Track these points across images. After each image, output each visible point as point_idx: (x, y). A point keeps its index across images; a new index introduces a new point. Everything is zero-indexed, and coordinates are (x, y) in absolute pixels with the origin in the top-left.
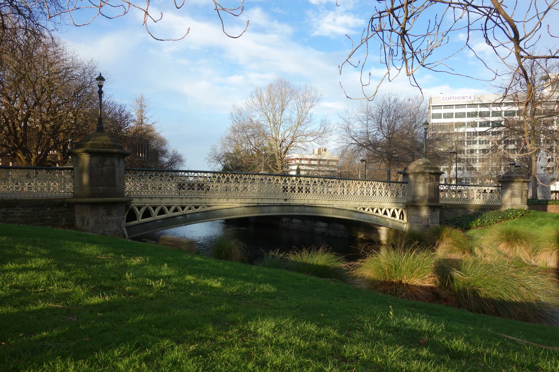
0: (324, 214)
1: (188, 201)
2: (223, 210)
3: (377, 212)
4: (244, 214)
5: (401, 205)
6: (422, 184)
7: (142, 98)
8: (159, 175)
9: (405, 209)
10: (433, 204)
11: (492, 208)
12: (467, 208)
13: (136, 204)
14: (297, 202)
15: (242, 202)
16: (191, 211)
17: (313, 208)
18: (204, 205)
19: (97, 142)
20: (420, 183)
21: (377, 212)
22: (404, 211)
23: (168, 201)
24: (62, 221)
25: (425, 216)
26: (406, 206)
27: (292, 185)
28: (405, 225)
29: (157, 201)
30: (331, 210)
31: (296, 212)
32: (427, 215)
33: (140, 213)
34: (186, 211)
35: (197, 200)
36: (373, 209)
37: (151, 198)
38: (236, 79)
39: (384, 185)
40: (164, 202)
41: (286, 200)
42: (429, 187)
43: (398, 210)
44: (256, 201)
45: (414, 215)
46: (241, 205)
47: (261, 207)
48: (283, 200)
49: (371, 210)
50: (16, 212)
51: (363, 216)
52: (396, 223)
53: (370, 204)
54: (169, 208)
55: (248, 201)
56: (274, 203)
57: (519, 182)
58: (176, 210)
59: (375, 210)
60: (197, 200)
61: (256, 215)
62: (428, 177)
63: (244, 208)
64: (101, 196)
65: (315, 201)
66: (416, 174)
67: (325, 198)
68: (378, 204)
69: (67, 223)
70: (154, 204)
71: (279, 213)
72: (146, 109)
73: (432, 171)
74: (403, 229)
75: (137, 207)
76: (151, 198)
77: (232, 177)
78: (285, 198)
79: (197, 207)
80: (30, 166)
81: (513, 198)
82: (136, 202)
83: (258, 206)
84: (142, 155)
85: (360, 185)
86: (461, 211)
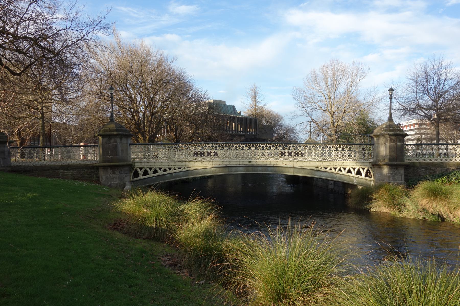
0: (286, 172)
1: (173, 164)
2: (199, 170)
3: (340, 170)
4: (216, 173)
5: (368, 164)
6: (383, 145)
7: (255, 87)
8: (174, 147)
9: (371, 168)
10: (392, 163)
12: (446, 166)
13: (138, 167)
16: (175, 171)
17: (275, 168)
18: (184, 166)
19: (107, 128)
20: (382, 144)
21: (340, 170)
22: (370, 170)
23: (159, 164)
24: (94, 177)
25: (387, 174)
26: (373, 166)
28: (372, 182)
29: (153, 164)
30: (292, 170)
32: (388, 173)
33: (141, 173)
34: (172, 171)
35: (180, 164)
36: (335, 169)
37: (148, 162)
39: (347, 147)
40: (156, 165)
41: (250, 162)
42: (390, 148)
43: (363, 169)
44: (225, 163)
45: (378, 173)
46: (212, 166)
47: (229, 168)
48: (248, 162)
49: (333, 170)
50: (68, 172)
51: (325, 174)
52: (361, 180)
53: (332, 164)
54: (160, 169)
55: (218, 163)
56: (240, 165)
58: (165, 170)
59: (337, 169)
60: (180, 164)
61: (260, 172)
62: (389, 139)
63: (215, 168)
64: (109, 161)
65: (277, 162)
66: (379, 136)
67: (346, 160)
68: (341, 164)
69: (97, 178)
70: (150, 167)
71: (245, 172)
72: (258, 95)
73: (391, 133)
74: (370, 186)
75: (139, 169)
76: (148, 162)
78: (249, 161)
79: (180, 168)
80: (145, 143)
82: (138, 166)
83: (226, 167)
84: (252, 130)
86: (440, 169)
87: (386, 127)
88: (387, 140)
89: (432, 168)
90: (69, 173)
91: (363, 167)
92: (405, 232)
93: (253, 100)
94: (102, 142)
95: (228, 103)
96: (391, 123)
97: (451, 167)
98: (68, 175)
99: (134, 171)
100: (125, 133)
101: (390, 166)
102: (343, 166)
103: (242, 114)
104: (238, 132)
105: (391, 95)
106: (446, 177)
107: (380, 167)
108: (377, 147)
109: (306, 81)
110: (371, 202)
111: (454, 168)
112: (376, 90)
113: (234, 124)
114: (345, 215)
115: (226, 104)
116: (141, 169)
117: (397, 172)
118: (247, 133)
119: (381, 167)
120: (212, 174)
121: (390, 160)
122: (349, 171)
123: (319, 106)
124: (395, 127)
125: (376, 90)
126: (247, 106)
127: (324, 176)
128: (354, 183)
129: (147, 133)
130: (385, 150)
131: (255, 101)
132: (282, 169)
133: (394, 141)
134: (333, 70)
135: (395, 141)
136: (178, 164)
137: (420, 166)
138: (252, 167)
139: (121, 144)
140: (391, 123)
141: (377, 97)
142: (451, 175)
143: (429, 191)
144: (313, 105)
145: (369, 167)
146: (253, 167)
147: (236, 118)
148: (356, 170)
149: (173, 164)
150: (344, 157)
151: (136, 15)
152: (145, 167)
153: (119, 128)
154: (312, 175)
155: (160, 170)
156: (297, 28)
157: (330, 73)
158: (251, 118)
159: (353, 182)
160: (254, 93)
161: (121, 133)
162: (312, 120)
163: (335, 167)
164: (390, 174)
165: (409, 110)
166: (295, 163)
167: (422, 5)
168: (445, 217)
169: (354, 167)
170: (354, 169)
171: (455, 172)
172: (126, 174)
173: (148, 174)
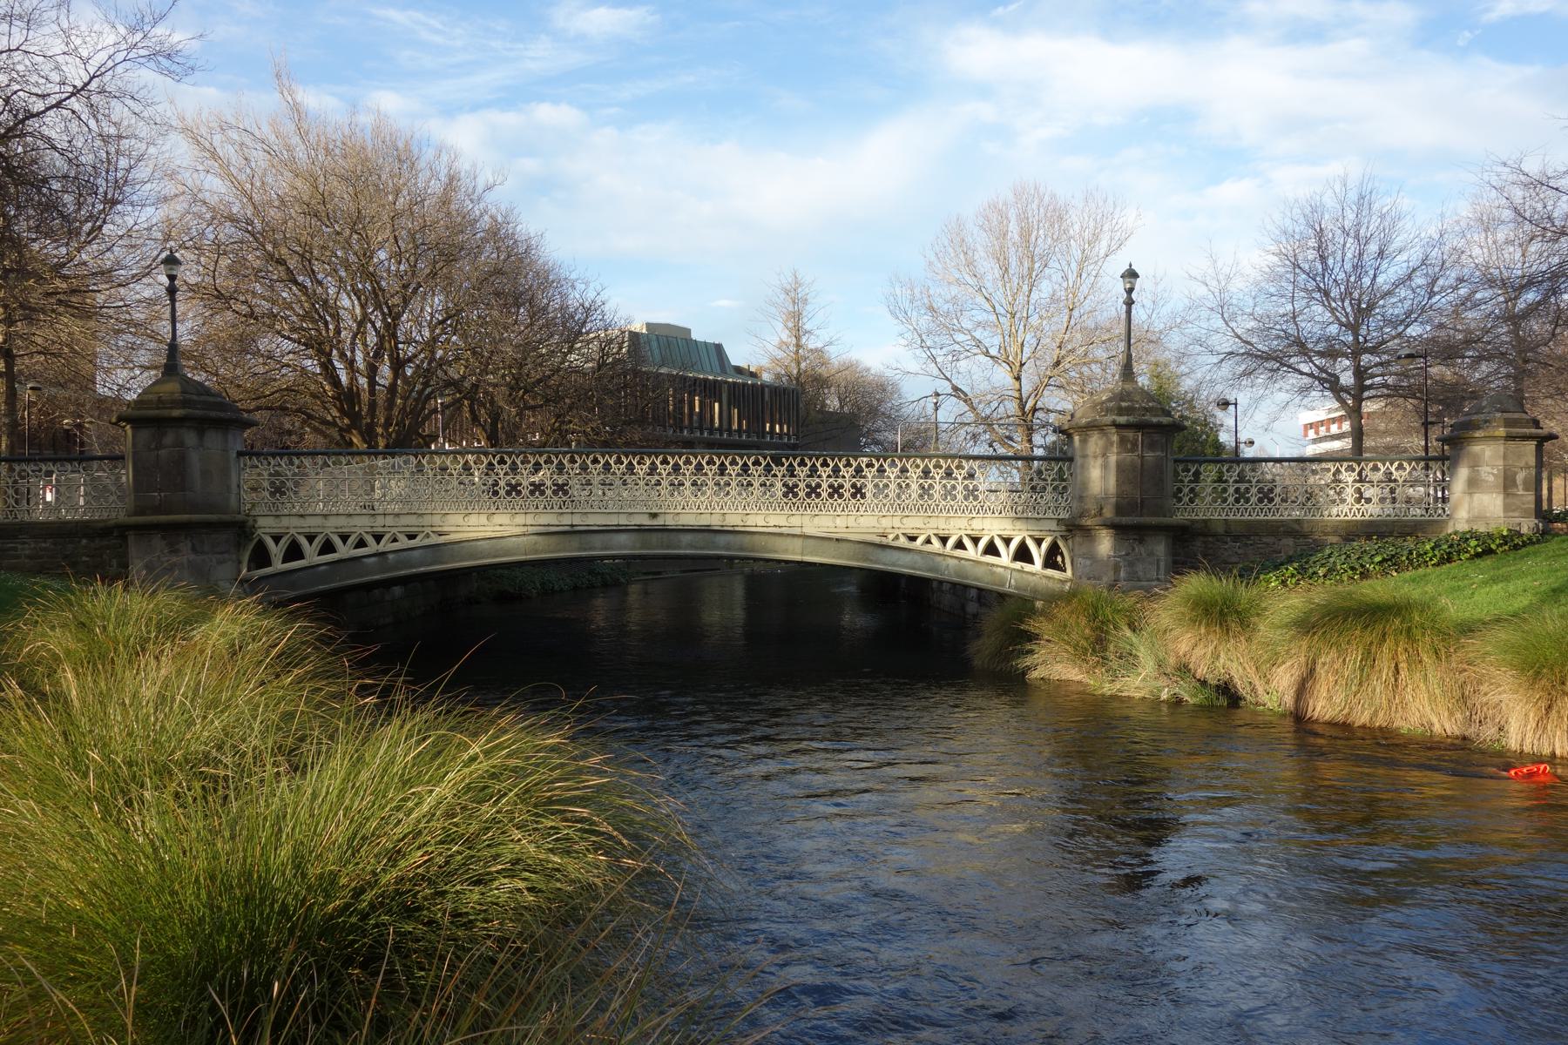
0: (776, 552)
1: (389, 521)
3: (960, 545)
4: (536, 552)
5: (1053, 526)
6: (1100, 461)
7: (797, 284)
10: (1125, 520)
11: (1408, 530)
13: (268, 530)
14: (688, 520)
15: (529, 522)
16: (396, 546)
18: (428, 530)
20: (1095, 457)
21: (960, 545)
22: (1061, 544)
23: (342, 521)
30: (798, 542)
31: (685, 546)
33: (276, 551)
34: (385, 545)
36: (944, 540)
37: (302, 516)
38: (1233, 191)
40: (331, 527)
41: (654, 516)
42: (1119, 465)
43: (1039, 542)
45: (1084, 556)
46: (525, 529)
47: (583, 536)
49: (936, 544)
50: (20, 546)
53: (933, 523)
55: (544, 519)
58: (361, 543)
59: (951, 543)
62: (1115, 438)
63: (535, 537)
64: (157, 510)
65: (745, 518)
68: (962, 523)
70: (307, 530)
72: (808, 308)
73: (1122, 420)
76: (302, 516)
77: (665, 462)
79: (412, 537)
81: (1476, 496)
82: (266, 525)
84: (781, 429)
86: (1290, 541)
87: (1110, 400)
88: (1112, 444)
89: (1265, 540)
90: (23, 549)
91: (1037, 534)
92: (291, 613)
93: (790, 325)
94: (134, 445)
96: (1126, 386)
97: (1326, 534)
98: (18, 557)
99: (251, 547)
100: (213, 414)
101: (1119, 530)
102: (970, 532)
103: (767, 377)
104: (711, 433)
105: (1130, 291)
106: (1296, 565)
107: (1087, 532)
108: (1083, 466)
109: (933, 258)
110: (1028, 647)
111: (1334, 539)
112: (1160, 288)
113: (717, 405)
114: (974, 698)
116: (277, 539)
117: (1140, 550)
118: (763, 437)
119: (1093, 533)
120: (523, 558)
121: (1119, 510)
122: (991, 549)
123: (978, 343)
124: (1137, 398)
125: (1160, 288)
126: (770, 348)
128: (1006, 589)
130: (1104, 478)
131: (798, 332)
133: (1135, 445)
134: (1023, 218)
137: (1228, 533)
138: (660, 535)
139: (201, 452)
140: (1126, 386)
141: (1165, 311)
142: (1313, 559)
144: (958, 340)
145: (1058, 534)
146: (665, 535)
149: (389, 521)
151: (438, 39)
152: (292, 531)
153: (195, 397)
154: (864, 561)
155: (344, 543)
156: (983, 91)
157: (1014, 229)
158: (776, 388)
159: (1003, 585)
161: (198, 413)
162: (956, 389)
163: (941, 533)
164: (1120, 557)
165: (1266, 357)
166: (806, 520)
167: (1404, 16)
168: (1242, 692)
169: (1006, 534)
170: (1007, 541)
171: (1328, 552)
172: (222, 553)
173: (301, 556)
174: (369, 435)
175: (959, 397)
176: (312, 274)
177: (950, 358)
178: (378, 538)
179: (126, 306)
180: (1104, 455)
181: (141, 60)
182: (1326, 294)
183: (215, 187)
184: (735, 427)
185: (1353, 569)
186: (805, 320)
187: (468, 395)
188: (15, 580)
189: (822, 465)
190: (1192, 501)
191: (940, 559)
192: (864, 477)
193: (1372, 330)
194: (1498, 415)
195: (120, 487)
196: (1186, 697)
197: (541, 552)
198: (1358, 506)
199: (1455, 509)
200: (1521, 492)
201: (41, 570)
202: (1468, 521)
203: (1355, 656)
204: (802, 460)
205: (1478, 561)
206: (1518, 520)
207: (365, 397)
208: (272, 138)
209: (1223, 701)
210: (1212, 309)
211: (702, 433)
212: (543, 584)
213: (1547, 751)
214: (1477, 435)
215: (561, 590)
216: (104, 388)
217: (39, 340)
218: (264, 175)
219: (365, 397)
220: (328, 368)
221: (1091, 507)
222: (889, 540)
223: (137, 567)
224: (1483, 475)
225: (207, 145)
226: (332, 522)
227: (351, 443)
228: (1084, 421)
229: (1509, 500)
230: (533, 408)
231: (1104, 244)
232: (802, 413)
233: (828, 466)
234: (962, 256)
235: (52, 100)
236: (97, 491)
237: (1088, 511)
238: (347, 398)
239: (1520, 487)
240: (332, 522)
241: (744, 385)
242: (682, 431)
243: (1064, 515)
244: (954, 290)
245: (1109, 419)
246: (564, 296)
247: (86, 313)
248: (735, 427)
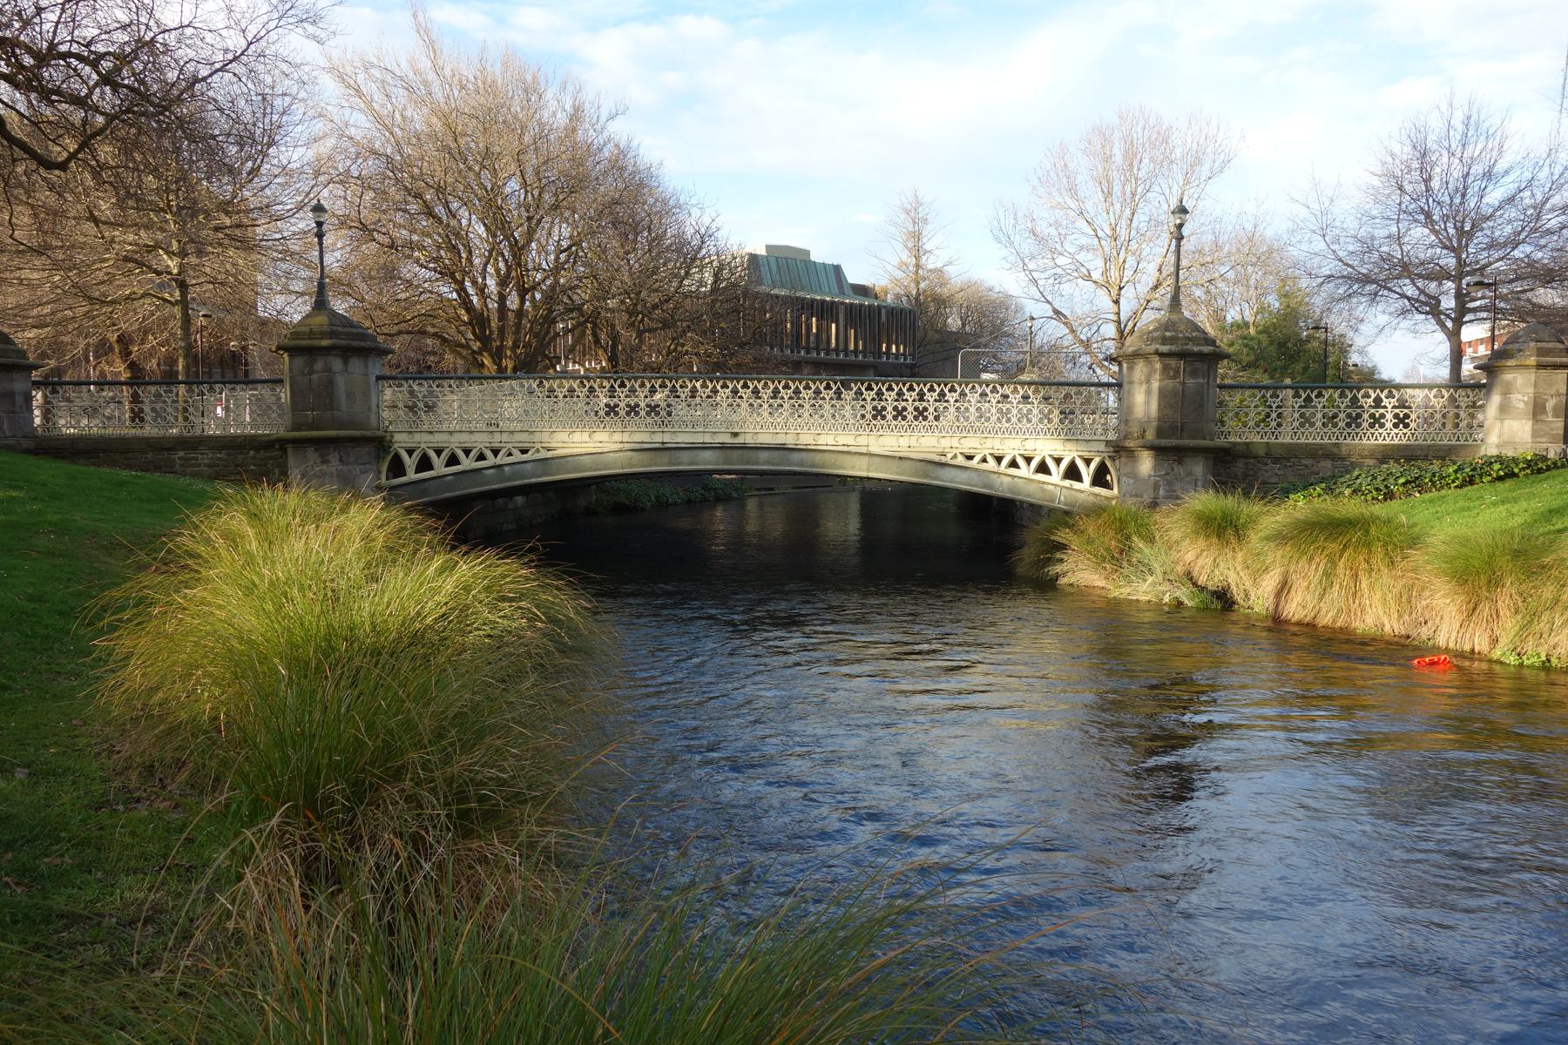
0: (844, 468)
1: (505, 437)
3: (1014, 464)
5: (1102, 447)
7: (919, 204)
10: (1164, 442)
14: (766, 439)
17: (812, 454)
18: (538, 446)
22: (1109, 464)
27: (1397, 411)
30: (864, 461)
31: (763, 463)
33: (410, 462)
34: (502, 459)
36: (999, 459)
40: (455, 443)
41: (735, 435)
42: (1163, 394)
43: (1088, 462)
46: (620, 446)
49: (992, 463)
53: (989, 443)
57: (1526, 367)
58: (481, 457)
59: (1005, 462)
60: (524, 437)
62: (1158, 366)
64: (311, 427)
72: (929, 227)
73: (1165, 349)
79: (524, 451)
81: (1507, 422)
82: (401, 441)
84: (897, 349)
85: (914, 394)
86: (1328, 464)
87: (1156, 330)
88: (1155, 371)
89: (1303, 462)
91: (1087, 455)
92: (406, 508)
93: (910, 245)
94: (291, 370)
95: (817, 256)
98: (199, 465)
100: (356, 343)
101: (1159, 451)
103: (890, 299)
105: (1180, 226)
106: (1323, 485)
108: (1129, 391)
110: (1058, 555)
113: (834, 326)
115: (813, 258)
116: (410, 452)
118: (880, 357)
121: (1160, 433)
122: (1043, 468)
124: (1182, 328)
126: (890, 268)
127: (960, 481)
128: (1056, 505)
129: (509, 353)
130: (1147, 403)
131: (918, 252)
132: (818, 457)
133: (1177, 372)
135: (1178, 372)
136: (518, 437)
138: (740, 452)
139: (348, 376)
142: (1342, 480)
143: (1200, 519)
145: (1106, 455)
146: (745, 452)
147: (842, 309)
148: (1064, 464)
149: (505, 437)
150: (1025, 425)
152: (423, 446)
153: (340, 329)
159: (1053, 501)
160: (914, 222)
161: (343, 342)
162: (1057, 312)
163: (997, 453)
165: (1366, 280)
166: (872, 440)
169: (1057, 454)
170: (1058, 461)
174: (498, 356)
175: (1059, 320)
176: (447, 205)
177: (1051, 281)
178: (496, 452)
179: (284, 238)
180: (1148, 381)
181: (290, 27)
182: (1428, 215)
183: (361, 125)
184: (852, 347)
185: (1377, 489)
186: (925, 240)
187: (590, 322)
188: (199, 485)
189: (887, 390)
190: (1279, 425)
191: (994, 477)
192: (947, 401)
193: (1475, 251)
194: (1532, 344)
195: (280, 406)
196: (1187, 602)
197: (636, 466)
198: (1396, 431)
199: (1487, 434)
200: (1550, 419)
201: (217, 476)
202: (1498, 446)
203: (1321, 562)
204: (870, 385)
205: (1499, 485)
206: (1545, 446)
207: (494, 323)
208: (411, 75)
209: (1218, 605)
210: (1314, 232)
211: (818, 354)
212: (657, 497)
213: (1467, 648)
214: (1509, 364)
215: (675, 504)
216: (264, 310)
217: (208, 270)
218: (405, 108)
219: (494, 323)
220: (461, 290)
221: (1135, 430)
222: (948, 459)
223: (295, 474)
224: (1515, 403)
225: (352, 83)
226: (457, 438)
227: (482, 365)
228: (1131, 349)
229: (1538, 426)
230: (650, 331)
231: (1206, 166)
232: (919, 334)
233: (893, 390)
234: (1065, 180)
235: (218, 66)
236: (261, 409)
237: (1131, 433)
238: (479, 321)
239: (1550, 414)
240: (457, 438)
241: (861, 306)
242: (799, 352)
243: (1112, 436)
244: (1059, 214)
245: (1152, 348)
246: (681, 224)
247: (246, 245)
248: (852, 347)
